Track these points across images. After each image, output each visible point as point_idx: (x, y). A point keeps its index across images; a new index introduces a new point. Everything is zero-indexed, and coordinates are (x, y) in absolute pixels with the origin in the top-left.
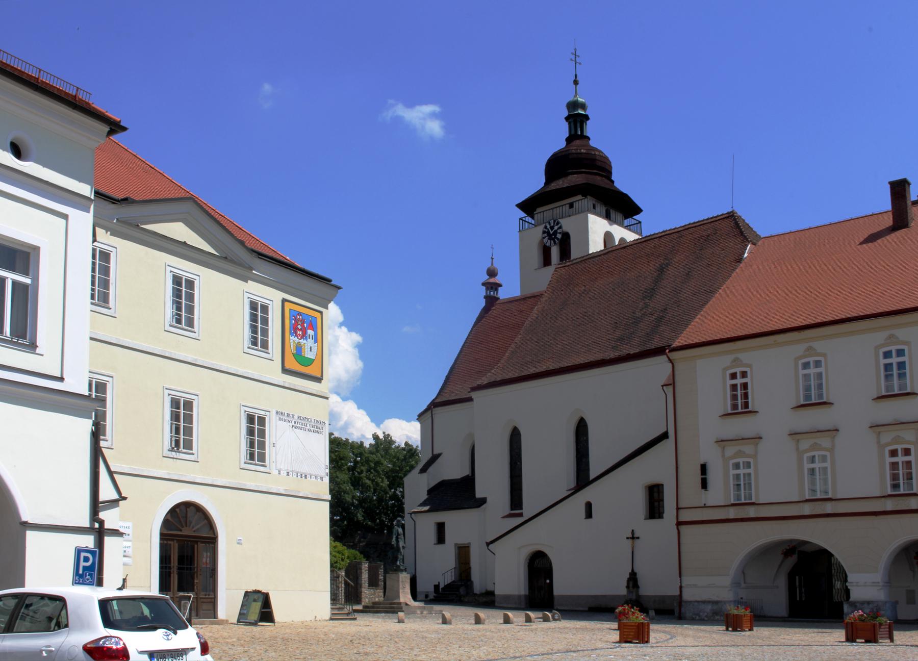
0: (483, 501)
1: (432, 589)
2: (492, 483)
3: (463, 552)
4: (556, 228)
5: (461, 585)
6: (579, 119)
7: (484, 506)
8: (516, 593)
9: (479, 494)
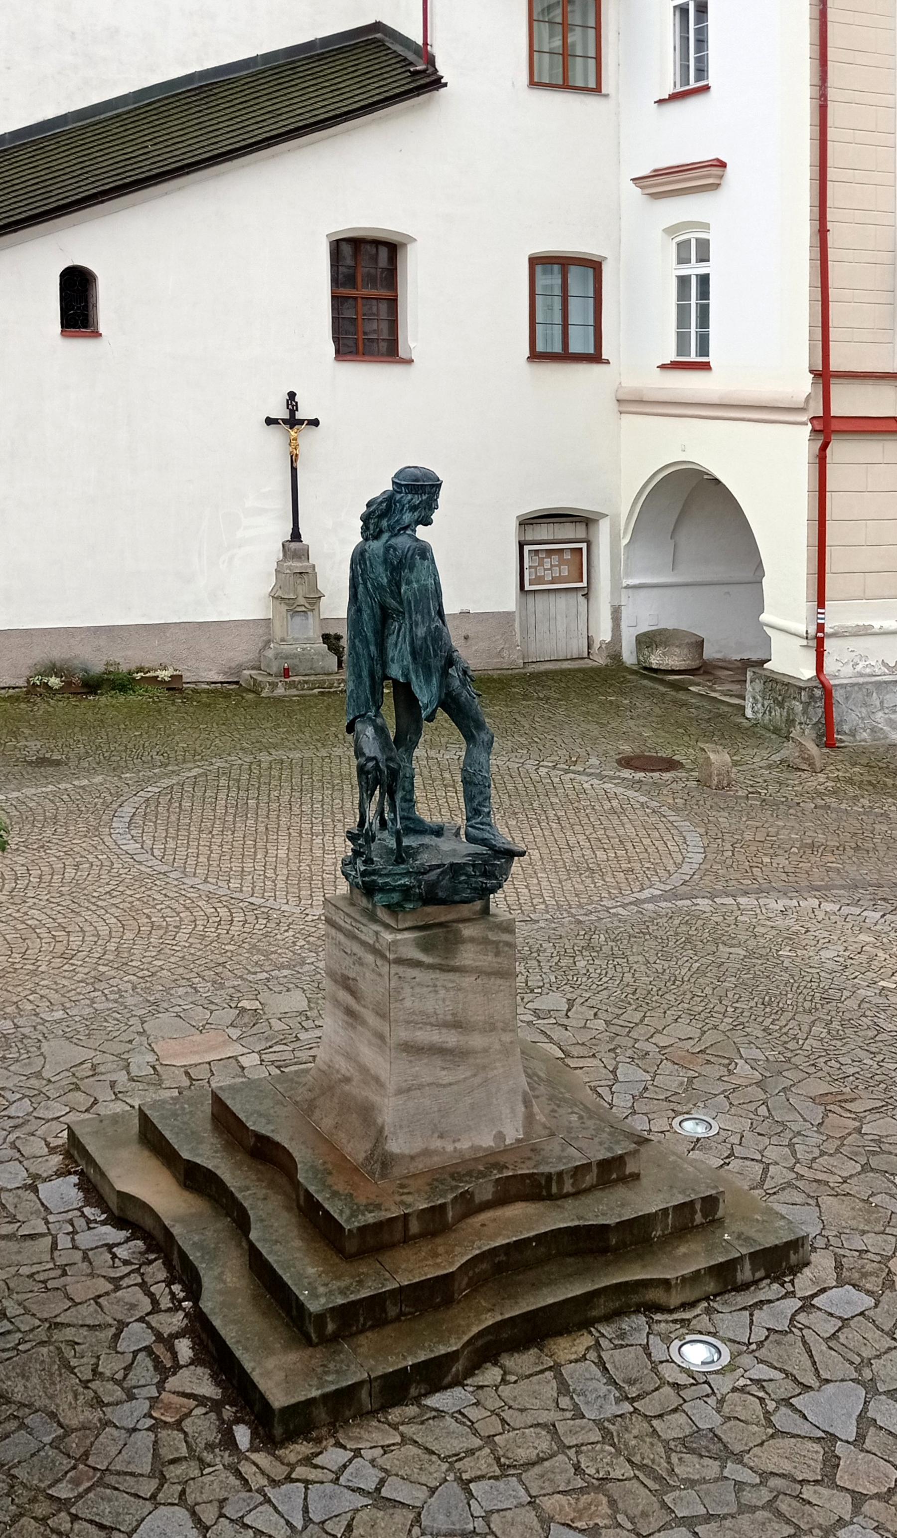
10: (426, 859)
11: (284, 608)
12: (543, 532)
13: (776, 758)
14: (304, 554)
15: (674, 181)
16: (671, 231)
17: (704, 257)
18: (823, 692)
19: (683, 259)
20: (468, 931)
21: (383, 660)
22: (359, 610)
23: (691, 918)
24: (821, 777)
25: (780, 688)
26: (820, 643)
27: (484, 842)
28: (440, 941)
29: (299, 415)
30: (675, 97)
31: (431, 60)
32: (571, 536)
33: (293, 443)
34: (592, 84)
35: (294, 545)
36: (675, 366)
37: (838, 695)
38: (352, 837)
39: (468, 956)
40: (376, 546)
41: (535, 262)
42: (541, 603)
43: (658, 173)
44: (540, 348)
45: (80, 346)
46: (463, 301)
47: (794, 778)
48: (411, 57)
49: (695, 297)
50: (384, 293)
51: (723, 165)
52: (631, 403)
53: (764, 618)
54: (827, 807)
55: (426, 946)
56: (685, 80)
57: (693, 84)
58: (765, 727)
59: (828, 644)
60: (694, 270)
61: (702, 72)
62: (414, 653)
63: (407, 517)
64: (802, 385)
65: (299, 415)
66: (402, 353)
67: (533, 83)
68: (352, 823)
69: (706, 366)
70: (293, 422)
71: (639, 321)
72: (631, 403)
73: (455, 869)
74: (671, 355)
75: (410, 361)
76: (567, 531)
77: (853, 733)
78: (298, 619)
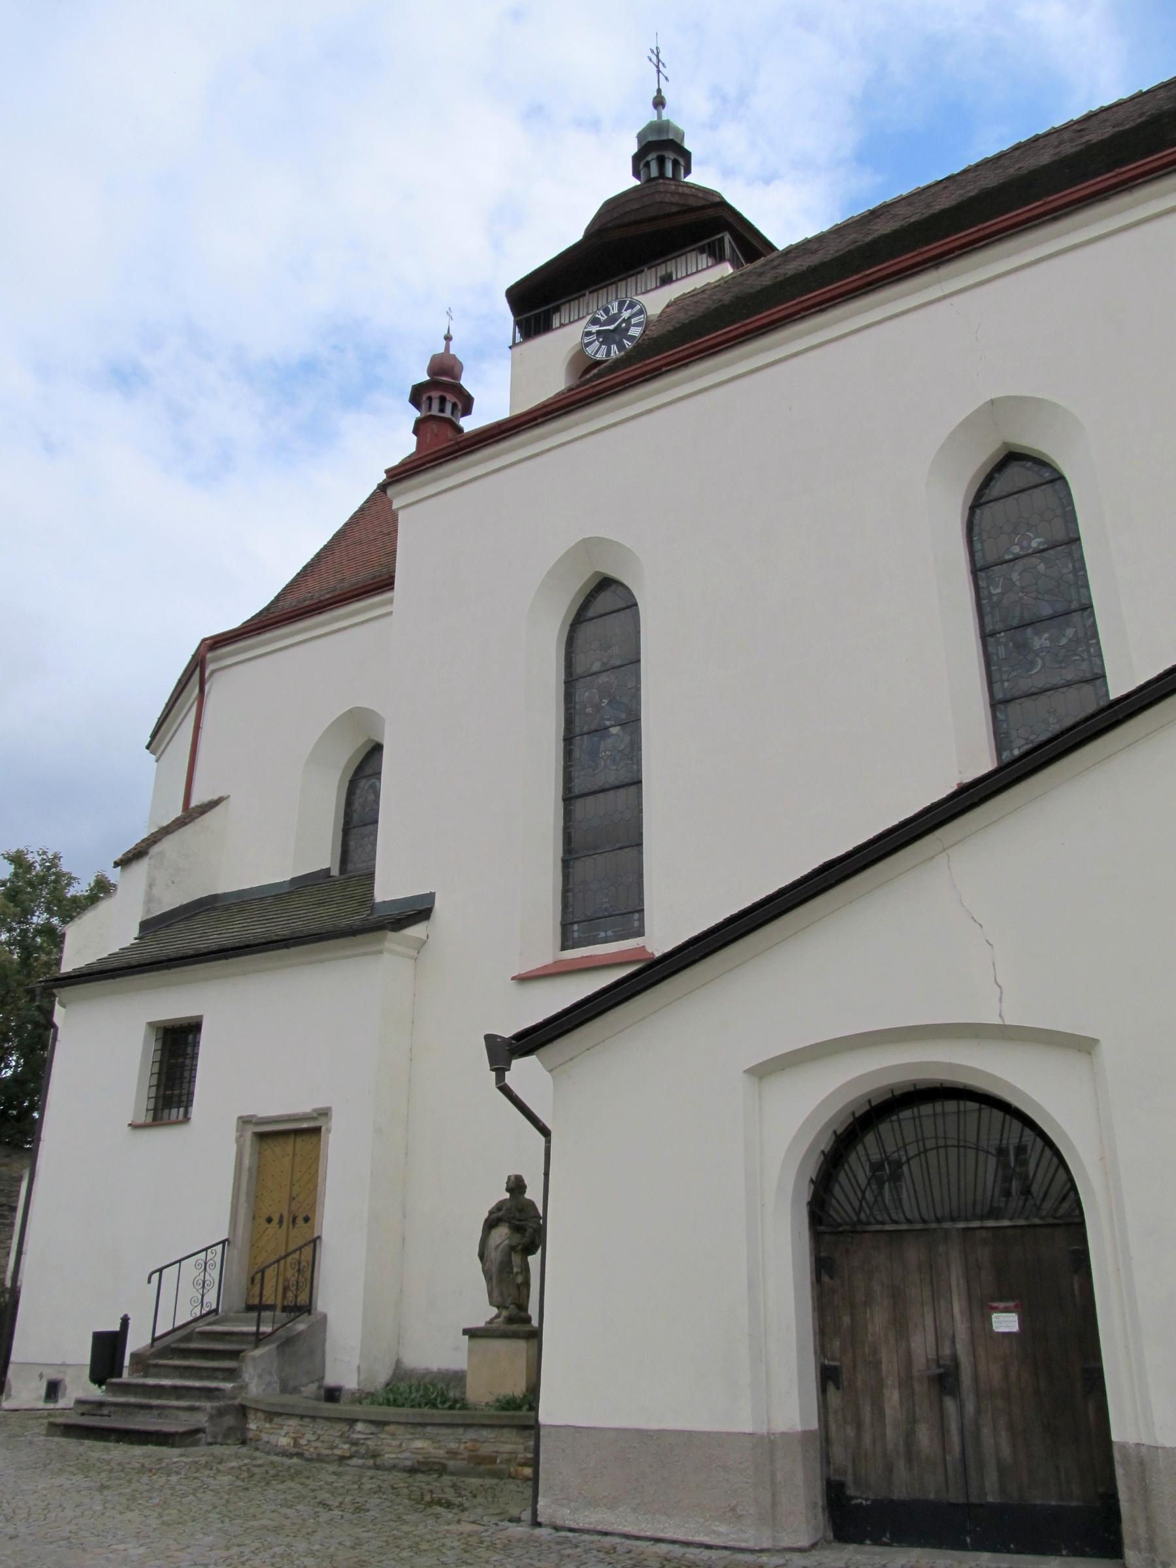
0: (418, 911)
1: (84, 1354)
3: (285, 1148)
4: (626, 314)
5: (259, 1339)
6: (670, 156)
7: (416, 931)
8: (744, 1423)
9: (389, 887)
10: (579, 327)
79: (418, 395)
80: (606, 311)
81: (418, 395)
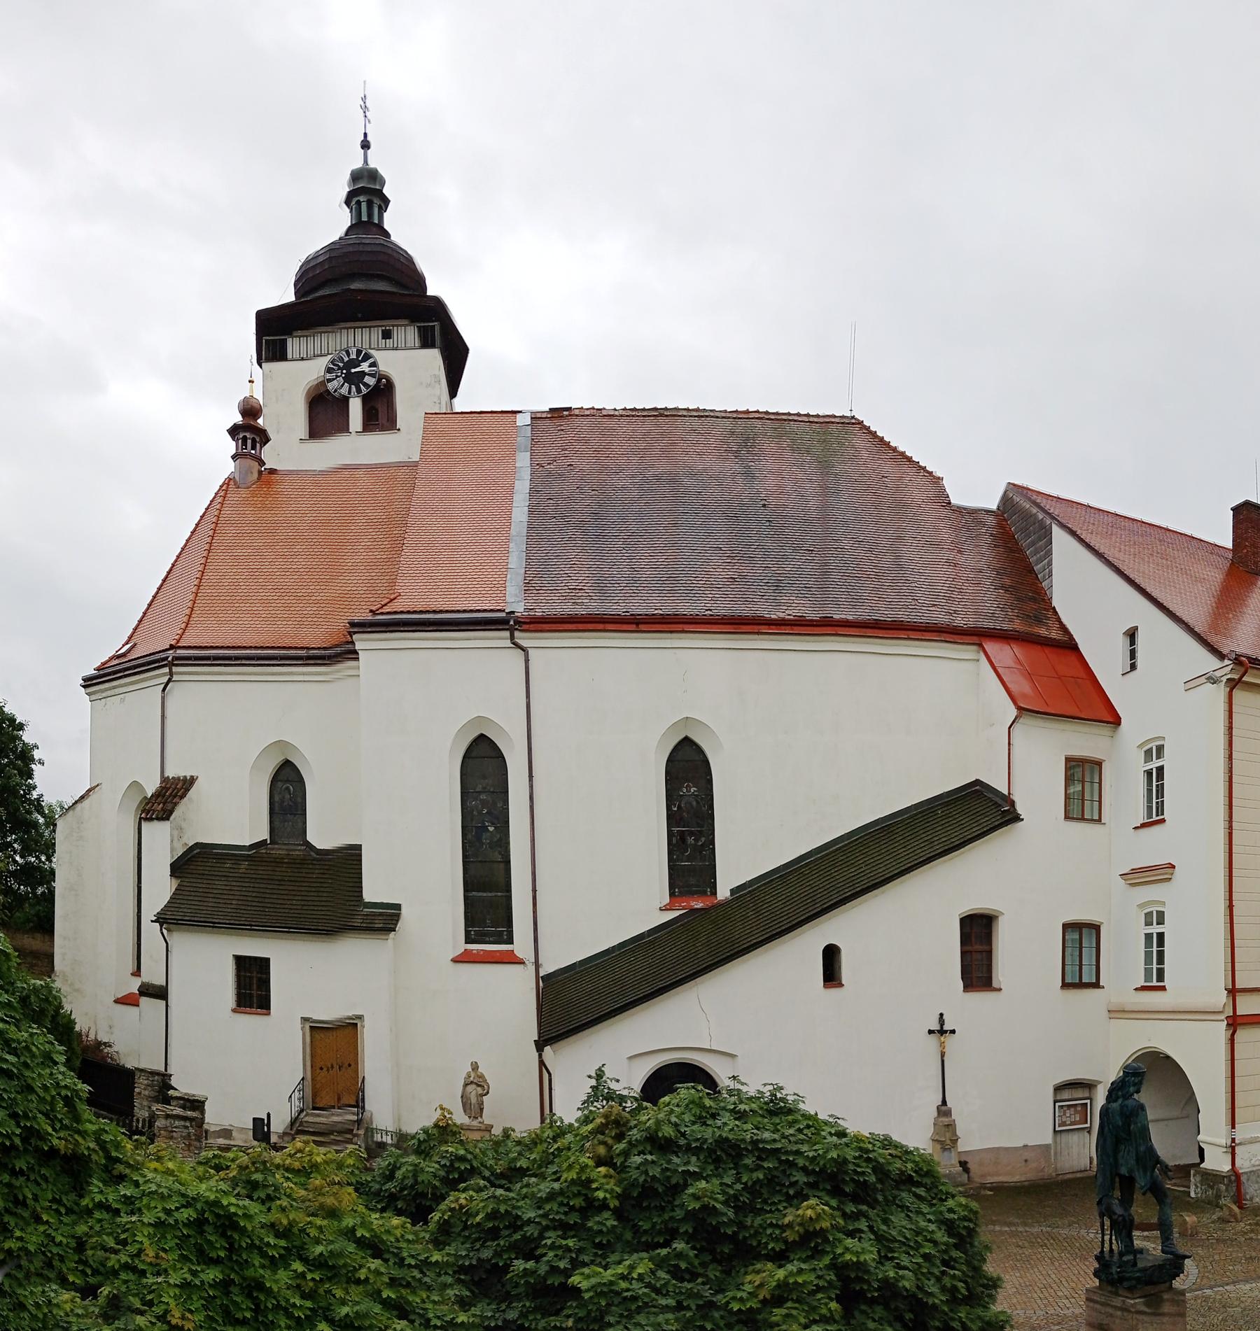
2: (414, 864)
6: (377, 201)
11: (938, 1146)
12: (1066, 1094)
13: (1215, 1217)
14: (948, 1113)
15: (1142, 876)
16: (1141, 906)
17: (1161, 921)
18: (1235, 1177)
19: (1148, 923)
20: (1166, 1296)
21: (1116, 1165)
22: (1105, 1140)
23: (1206, 1299)
24: (1242, 1224)
25: (1211, 1178)
26: (1233, 1148)
27: (1171, 1253)
28: (1154, 1302)
29: (945, 1028)
30: (1143, 826)
31: (1012, 803)
32: (1080, 1096)
33: (942, 1044)
34: (1096, 817)
35: (943, 1108)
36: (1144, 988)
37: (1243, 1178)
38: (1098, 1258)
39: (1167, 1308)
40: (1115, 1105)
41: (1067, 927)
42: (1064, 1137)
43: (1134, 871)
44: (1068, 980)
45: (834, 992)
46: (1026, 953)
47: (1228, 1227)
48: (1000, 802)
49: (1156, 944)
50: (986, 948)
51: (1173, 867)
52: (1116, 1013)
53: (1200, 1138)
54: (1251, 1239)
55: (1147, 1305)
56: (1150, 816)
57: (1155, 818)
58: (1203, 1201)
59: (1237, 1149)
60: (1155, 929)
61: (1160, 810)
62: (1137, 1160)
63: (1132, 1089)
64: (1222, 998)
65: (945, 1028)
66: (995, 985)
67: (1067, 817)
68: (1097, 1252)
69: (1163, 988)
70: (942, 1032)
71: (1122, 960)
72: (1116, 1013)
73: (1161, 1267)
74: (1142, 983)
75: (1000, 990)
76: (1079, 1093)
77: (1251, 1199)
78: (946, 1153)
79: (234, 431)
80: (348, 355)
81: (234, 431)
